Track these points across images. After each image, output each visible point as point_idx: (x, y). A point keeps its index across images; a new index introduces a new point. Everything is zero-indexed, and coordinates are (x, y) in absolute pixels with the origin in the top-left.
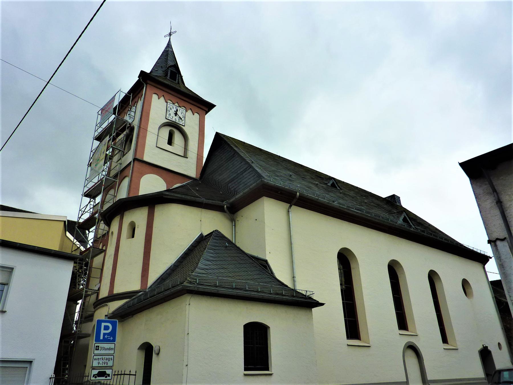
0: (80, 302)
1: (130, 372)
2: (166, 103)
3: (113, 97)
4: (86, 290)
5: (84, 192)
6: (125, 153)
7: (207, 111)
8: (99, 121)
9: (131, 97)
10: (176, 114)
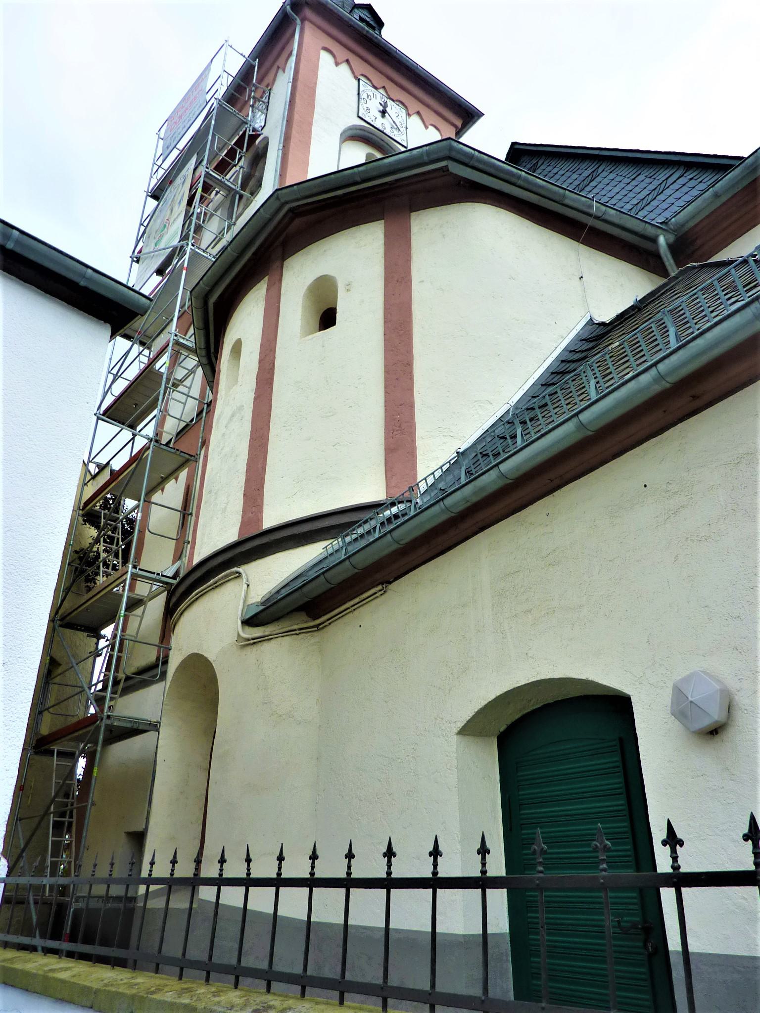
0: (108, 631)
1: (390, 853)
2: (356, 82)
3: (207, 66)
4: (134, 571)
5: (82, 504)
6: (122, 585)
7: (460, 127)
8: (160, 151)
9: (254, 67)
10: (383, 113)
